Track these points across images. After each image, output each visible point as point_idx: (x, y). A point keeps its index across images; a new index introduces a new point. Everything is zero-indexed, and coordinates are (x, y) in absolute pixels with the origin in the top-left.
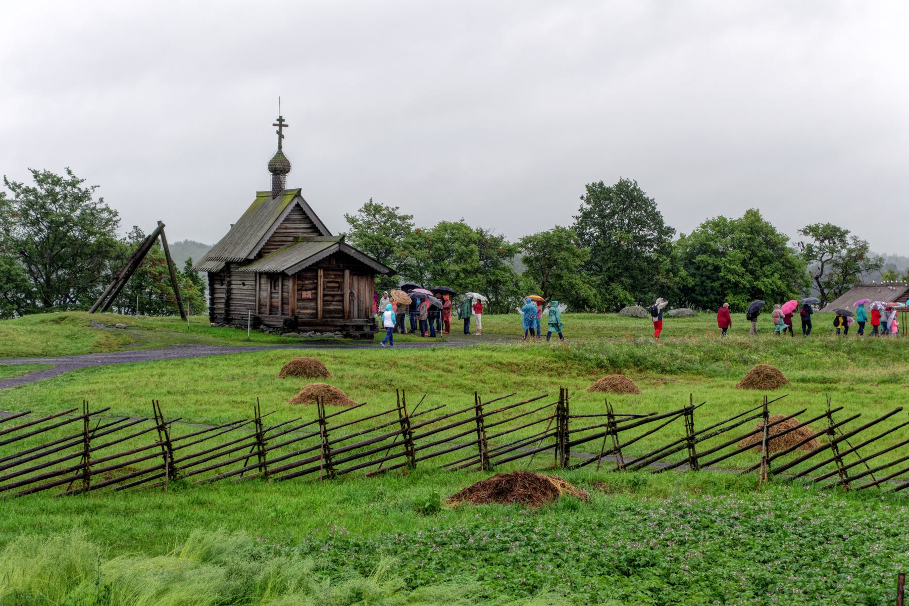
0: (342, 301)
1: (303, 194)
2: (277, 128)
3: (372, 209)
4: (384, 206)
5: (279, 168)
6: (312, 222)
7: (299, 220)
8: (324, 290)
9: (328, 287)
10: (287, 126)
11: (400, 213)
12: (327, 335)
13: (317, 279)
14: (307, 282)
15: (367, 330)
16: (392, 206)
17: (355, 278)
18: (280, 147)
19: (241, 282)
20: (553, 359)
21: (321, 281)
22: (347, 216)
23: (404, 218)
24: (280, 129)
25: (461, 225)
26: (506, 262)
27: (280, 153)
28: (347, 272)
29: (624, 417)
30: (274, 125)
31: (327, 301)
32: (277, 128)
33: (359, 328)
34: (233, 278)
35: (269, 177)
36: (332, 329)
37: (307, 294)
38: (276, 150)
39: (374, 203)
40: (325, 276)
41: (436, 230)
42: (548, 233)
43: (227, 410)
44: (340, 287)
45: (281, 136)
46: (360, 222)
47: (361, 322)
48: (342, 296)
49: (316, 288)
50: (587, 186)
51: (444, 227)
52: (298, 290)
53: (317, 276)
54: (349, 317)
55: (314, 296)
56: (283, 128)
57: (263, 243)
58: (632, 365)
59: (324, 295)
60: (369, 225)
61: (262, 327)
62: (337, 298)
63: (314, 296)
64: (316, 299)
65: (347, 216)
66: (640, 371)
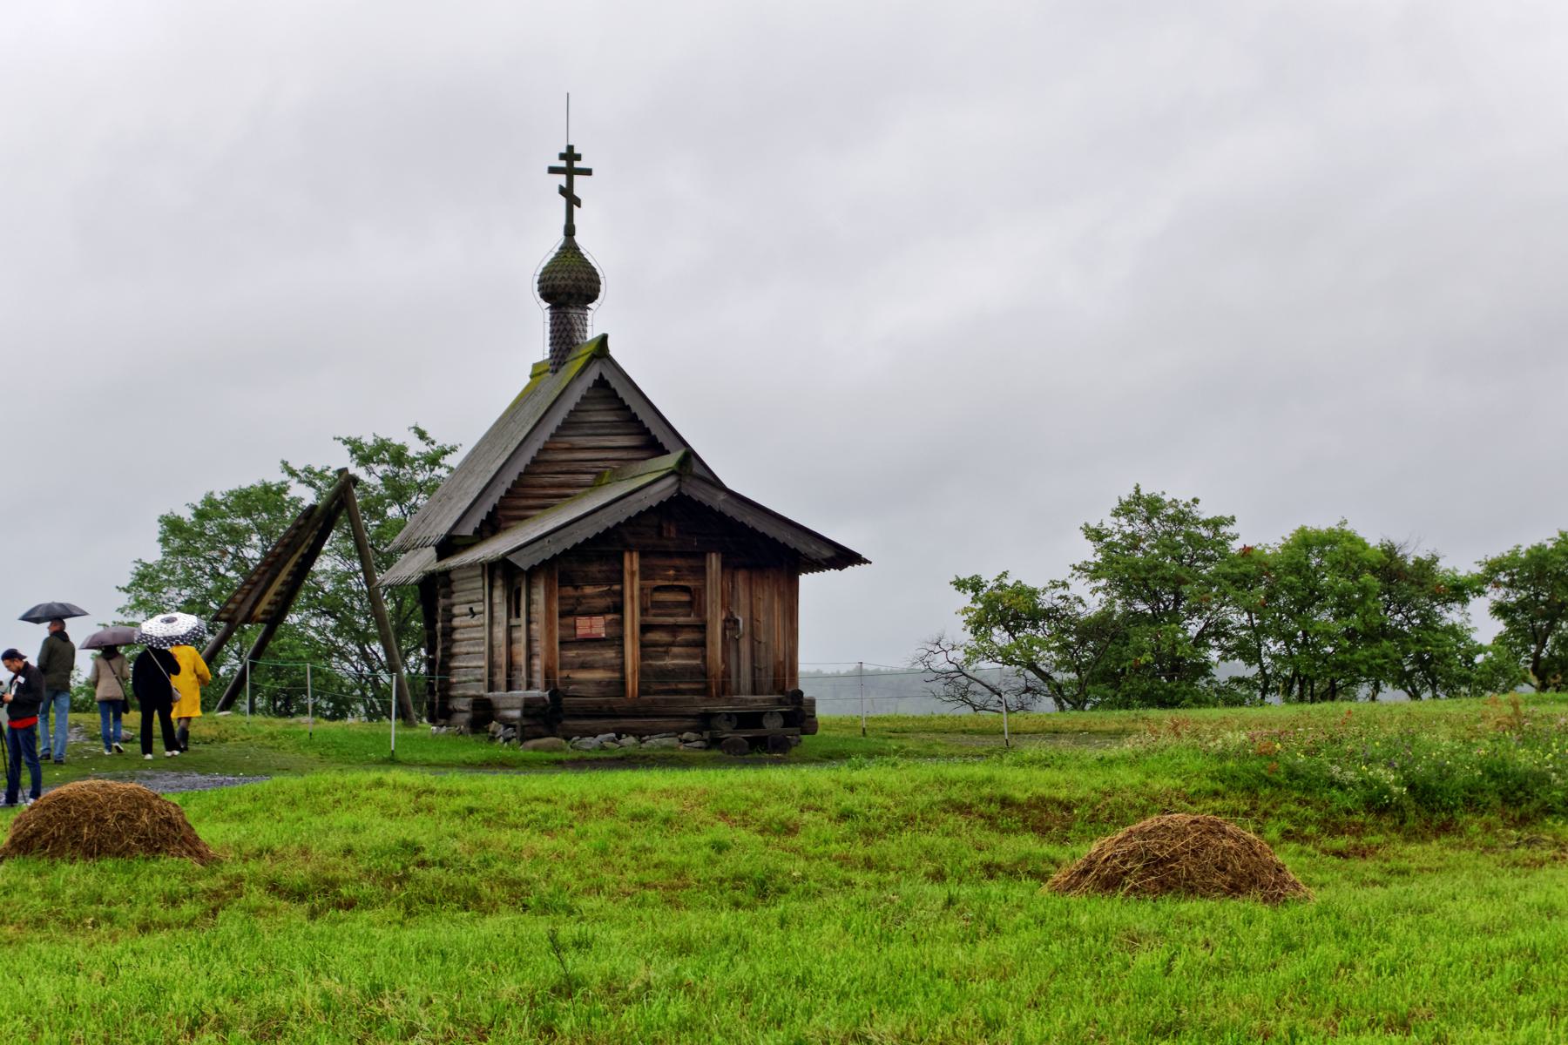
0: (702, 644)
1: (614, 350)
2: (561, 180)
3: (1144, 506)
4: (1167, 499)
5: (569, 286)
6: (647, 432)
7: (612, 424)
8: (644, 611)
9: (658, 605)
10: (588, 172)
11: (1205, 512)
12: (654, 743)
13: (621, 581)
14: (589, 590)
15: (773, 725)
16: (1185, 498)
17: (741, 577)
18: (570, 230)
20: (1209, 785)
21: (632, 588)
23: (1216, 524)
24: (570, 182)
25: (1342, 533)
26: (1452, 615)
27: (570, 247)
28: (714, 562)
30: (553, 170)
31: (655, 644)
32: (561, 180)
33: (751, 720)
34: (456, 598)
35: (541, 313)
36: (673, 723)
37: (596, 626)
38: (559, 238)
39: (1143, 493)
40: (646, 574)
41: (1286, 547)
42: (1540, 548)
44: (695, 602)
45: (572, 201)
46: (1117, 537)
47: (760, 702)
48: (702, 628)
49: (618, 609)
51: (1306, 541)
53: (621, 572)
54: (724, 690)
55: (613, 631)
56: (577, 178)
58: (1497, 801)
59: (645, 628)
60: (1134, 542)
61: (493, 725)
62: (684, 636)
63: (613, 631)
64: (621, 638)
66: (1523, 821)
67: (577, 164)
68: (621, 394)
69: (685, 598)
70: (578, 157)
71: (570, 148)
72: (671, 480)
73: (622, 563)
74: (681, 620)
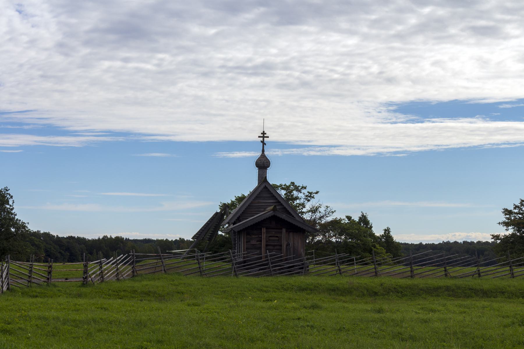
8: (267, 241)
10: (268, 137)
13: (261, 235)
14: (253, 236)
17: (291, 234)
18: (263, 151)
21: (264, 236)
24: (263, 139)
27: (263, 155)
28: (284, 230)
30: (259, 137)
32: (262, 139)
48: (281, 246)
52: (247, 242)
53: (261, 233)
57: (241, 212)
59: (267, 245)
67: (265, 135)
68: (270, 190)
69: (277, 239)
70: (266, 134)
71: (264, 132)
72: (272, 212)
73: (261, 230)
74: (275, 244)
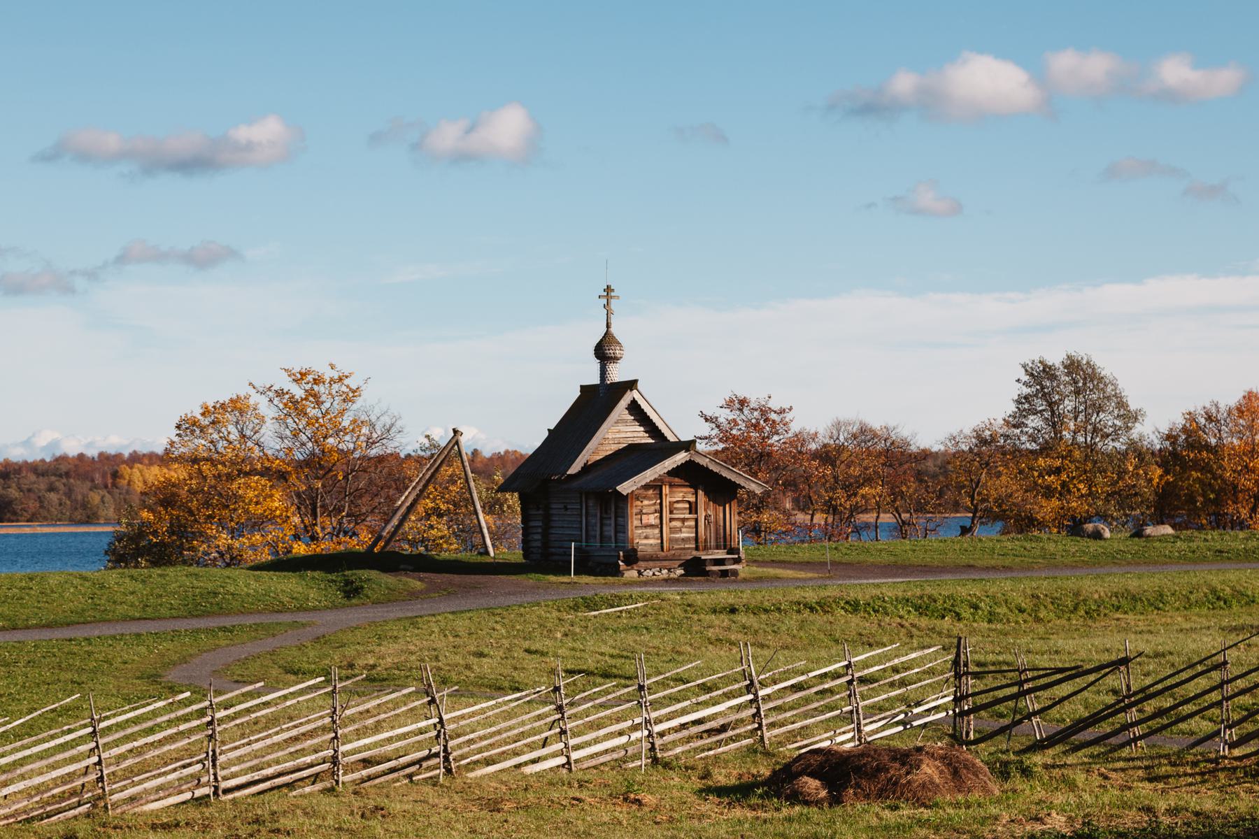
11: (774, 404)
14: (646, 502)
18: (608, 326)
19: (561, 506)
22: (702, 415)
29: (1041, 673)
35: (596, 365)
43: (1115, 770)
50: (1024, 366)
65: (702, 415)
